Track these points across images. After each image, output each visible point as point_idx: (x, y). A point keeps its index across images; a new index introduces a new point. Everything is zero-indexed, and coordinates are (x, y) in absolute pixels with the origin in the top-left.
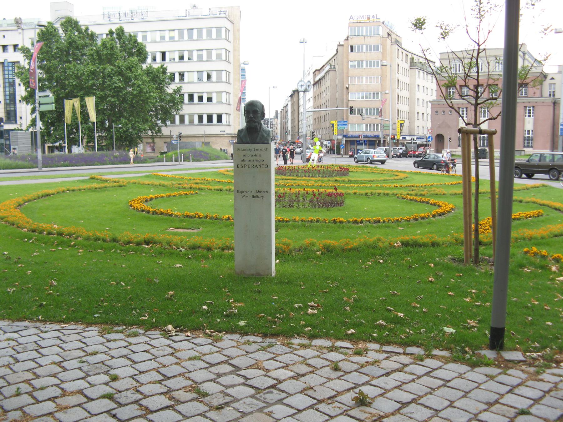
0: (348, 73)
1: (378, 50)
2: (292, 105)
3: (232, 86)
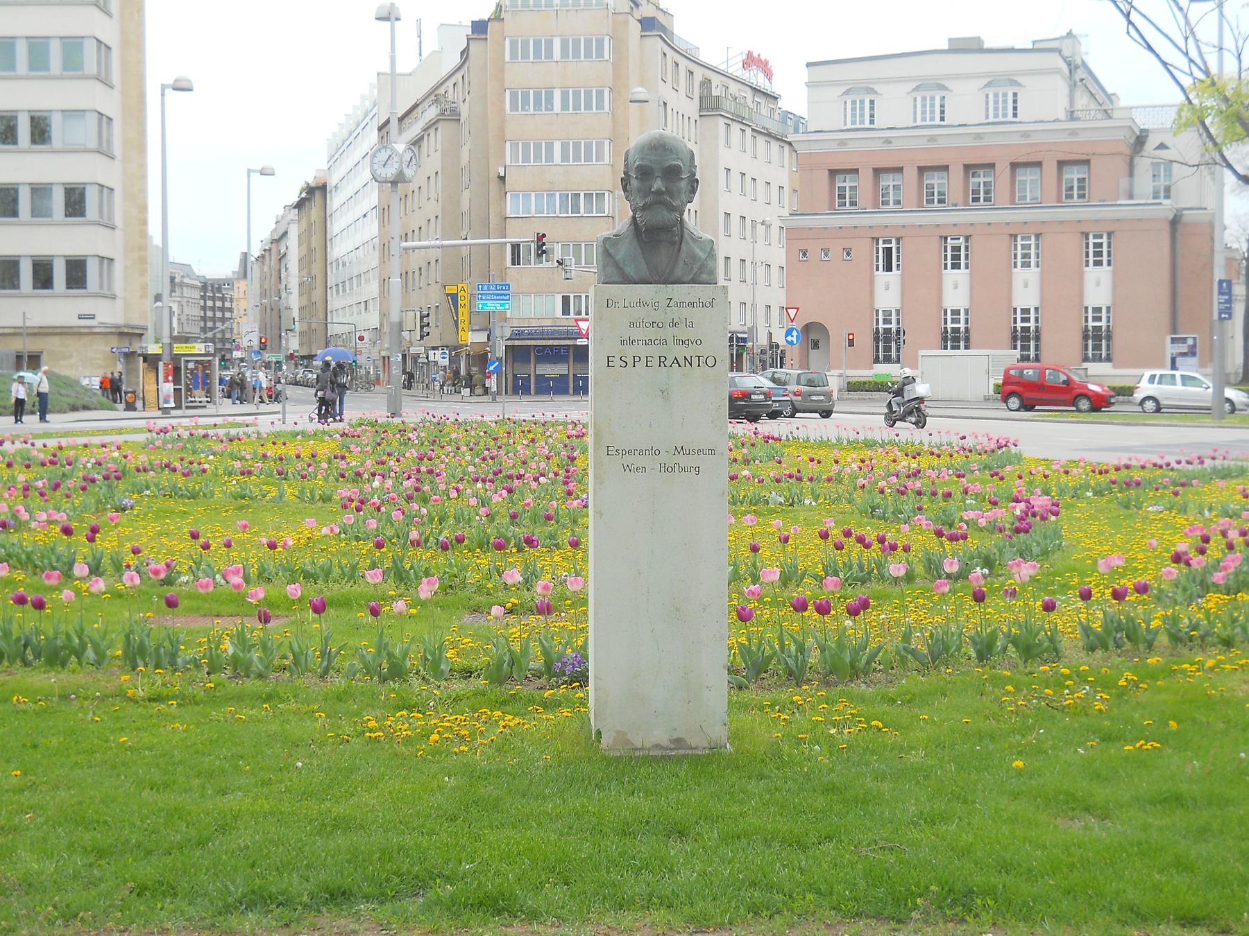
0: (502, 129)
1: (600, 53)
2: (305, 237)
3: (117, 163)
